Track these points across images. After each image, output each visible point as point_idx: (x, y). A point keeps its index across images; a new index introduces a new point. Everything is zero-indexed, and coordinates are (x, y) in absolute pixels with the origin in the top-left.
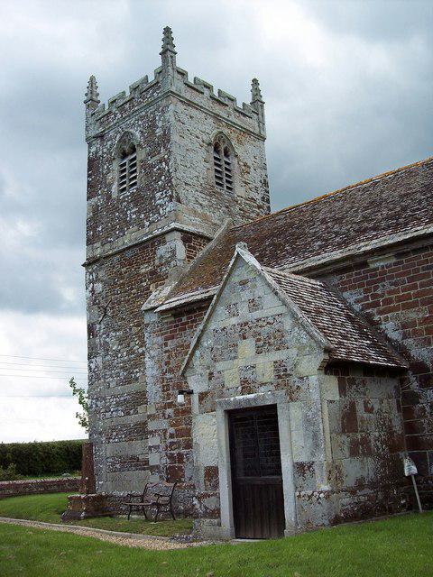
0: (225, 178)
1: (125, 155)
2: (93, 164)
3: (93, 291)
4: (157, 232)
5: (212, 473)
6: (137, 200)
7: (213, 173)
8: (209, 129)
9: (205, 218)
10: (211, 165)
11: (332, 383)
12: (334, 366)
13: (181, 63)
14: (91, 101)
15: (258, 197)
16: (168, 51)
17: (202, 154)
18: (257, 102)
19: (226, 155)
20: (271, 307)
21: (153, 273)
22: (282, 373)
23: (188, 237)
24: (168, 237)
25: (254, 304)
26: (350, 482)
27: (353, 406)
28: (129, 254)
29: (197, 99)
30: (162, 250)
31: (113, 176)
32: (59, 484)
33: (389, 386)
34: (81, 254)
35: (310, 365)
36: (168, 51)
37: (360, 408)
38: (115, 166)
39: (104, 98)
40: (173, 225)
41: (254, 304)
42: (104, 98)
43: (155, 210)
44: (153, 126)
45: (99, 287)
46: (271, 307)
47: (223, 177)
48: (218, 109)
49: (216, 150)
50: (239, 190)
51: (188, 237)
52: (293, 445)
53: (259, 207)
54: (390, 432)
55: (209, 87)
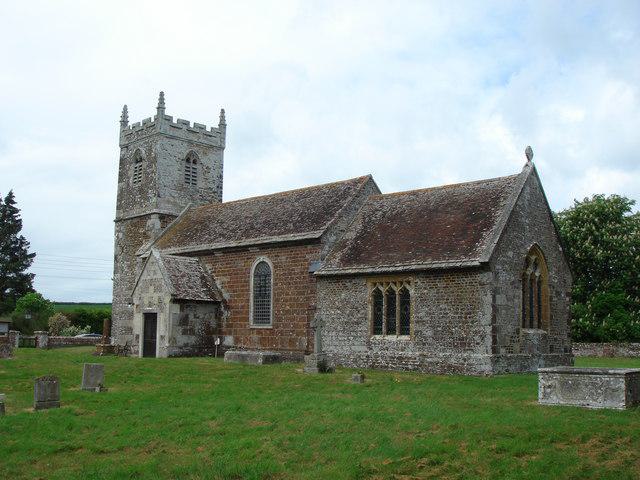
0: (191, 177)
1: (137, 162)
2: (122, 162)
3: (118, 237)
4: (148, 212)
5: (138, 336)
6: (141, 191)
7: (183, 177)
8: (184, 150)
9: (175, 204)
10: (183, 172)
11: (176, 308)
12: (175, 300)
13: (167, 112)
14: (124, 122)
15: (215, 187)
16: (161, 107)
17: (178, 166)
18: (223, 125)
19: (195, 162)
20: (159, 276)
21: (145, 234)
22: (160, 301)
23: (162, 217)
24: (152, 216)
25: (155, 273)
26: (181, 344)
27: (187, 316)
28: (135, 221)
29: (177, 133)
30: (149, 222)
31: (131, 173)
32: (388, 315)
33: (212, 308)
34: (114, 216)
35: (167, 299)
36: (161, 107)
37: (191, 317)
38: (132, 167)
39: (132, 122)
40: (155, 211)
41: (155, 273)
42: (132, 122)
43: (148, 199)
44: (150, 150)
45: (121, 235)
46: (159, 276)
47: (190, 177)
48: (191, 137)
49: (188, 160)
50: (201, 184)
51: (162, 217)
52: (162, 328)
53: (214, 192)
54: (208, 326)
55: (187, 123)
